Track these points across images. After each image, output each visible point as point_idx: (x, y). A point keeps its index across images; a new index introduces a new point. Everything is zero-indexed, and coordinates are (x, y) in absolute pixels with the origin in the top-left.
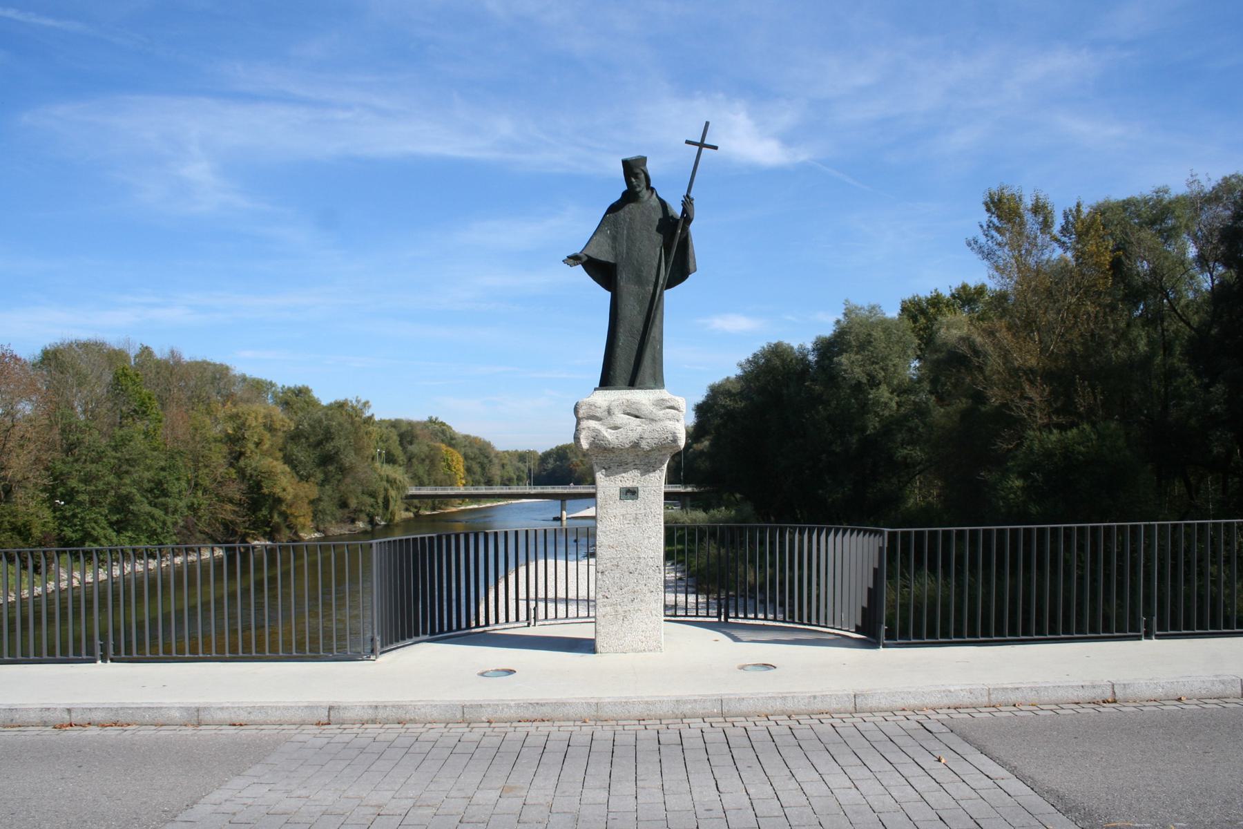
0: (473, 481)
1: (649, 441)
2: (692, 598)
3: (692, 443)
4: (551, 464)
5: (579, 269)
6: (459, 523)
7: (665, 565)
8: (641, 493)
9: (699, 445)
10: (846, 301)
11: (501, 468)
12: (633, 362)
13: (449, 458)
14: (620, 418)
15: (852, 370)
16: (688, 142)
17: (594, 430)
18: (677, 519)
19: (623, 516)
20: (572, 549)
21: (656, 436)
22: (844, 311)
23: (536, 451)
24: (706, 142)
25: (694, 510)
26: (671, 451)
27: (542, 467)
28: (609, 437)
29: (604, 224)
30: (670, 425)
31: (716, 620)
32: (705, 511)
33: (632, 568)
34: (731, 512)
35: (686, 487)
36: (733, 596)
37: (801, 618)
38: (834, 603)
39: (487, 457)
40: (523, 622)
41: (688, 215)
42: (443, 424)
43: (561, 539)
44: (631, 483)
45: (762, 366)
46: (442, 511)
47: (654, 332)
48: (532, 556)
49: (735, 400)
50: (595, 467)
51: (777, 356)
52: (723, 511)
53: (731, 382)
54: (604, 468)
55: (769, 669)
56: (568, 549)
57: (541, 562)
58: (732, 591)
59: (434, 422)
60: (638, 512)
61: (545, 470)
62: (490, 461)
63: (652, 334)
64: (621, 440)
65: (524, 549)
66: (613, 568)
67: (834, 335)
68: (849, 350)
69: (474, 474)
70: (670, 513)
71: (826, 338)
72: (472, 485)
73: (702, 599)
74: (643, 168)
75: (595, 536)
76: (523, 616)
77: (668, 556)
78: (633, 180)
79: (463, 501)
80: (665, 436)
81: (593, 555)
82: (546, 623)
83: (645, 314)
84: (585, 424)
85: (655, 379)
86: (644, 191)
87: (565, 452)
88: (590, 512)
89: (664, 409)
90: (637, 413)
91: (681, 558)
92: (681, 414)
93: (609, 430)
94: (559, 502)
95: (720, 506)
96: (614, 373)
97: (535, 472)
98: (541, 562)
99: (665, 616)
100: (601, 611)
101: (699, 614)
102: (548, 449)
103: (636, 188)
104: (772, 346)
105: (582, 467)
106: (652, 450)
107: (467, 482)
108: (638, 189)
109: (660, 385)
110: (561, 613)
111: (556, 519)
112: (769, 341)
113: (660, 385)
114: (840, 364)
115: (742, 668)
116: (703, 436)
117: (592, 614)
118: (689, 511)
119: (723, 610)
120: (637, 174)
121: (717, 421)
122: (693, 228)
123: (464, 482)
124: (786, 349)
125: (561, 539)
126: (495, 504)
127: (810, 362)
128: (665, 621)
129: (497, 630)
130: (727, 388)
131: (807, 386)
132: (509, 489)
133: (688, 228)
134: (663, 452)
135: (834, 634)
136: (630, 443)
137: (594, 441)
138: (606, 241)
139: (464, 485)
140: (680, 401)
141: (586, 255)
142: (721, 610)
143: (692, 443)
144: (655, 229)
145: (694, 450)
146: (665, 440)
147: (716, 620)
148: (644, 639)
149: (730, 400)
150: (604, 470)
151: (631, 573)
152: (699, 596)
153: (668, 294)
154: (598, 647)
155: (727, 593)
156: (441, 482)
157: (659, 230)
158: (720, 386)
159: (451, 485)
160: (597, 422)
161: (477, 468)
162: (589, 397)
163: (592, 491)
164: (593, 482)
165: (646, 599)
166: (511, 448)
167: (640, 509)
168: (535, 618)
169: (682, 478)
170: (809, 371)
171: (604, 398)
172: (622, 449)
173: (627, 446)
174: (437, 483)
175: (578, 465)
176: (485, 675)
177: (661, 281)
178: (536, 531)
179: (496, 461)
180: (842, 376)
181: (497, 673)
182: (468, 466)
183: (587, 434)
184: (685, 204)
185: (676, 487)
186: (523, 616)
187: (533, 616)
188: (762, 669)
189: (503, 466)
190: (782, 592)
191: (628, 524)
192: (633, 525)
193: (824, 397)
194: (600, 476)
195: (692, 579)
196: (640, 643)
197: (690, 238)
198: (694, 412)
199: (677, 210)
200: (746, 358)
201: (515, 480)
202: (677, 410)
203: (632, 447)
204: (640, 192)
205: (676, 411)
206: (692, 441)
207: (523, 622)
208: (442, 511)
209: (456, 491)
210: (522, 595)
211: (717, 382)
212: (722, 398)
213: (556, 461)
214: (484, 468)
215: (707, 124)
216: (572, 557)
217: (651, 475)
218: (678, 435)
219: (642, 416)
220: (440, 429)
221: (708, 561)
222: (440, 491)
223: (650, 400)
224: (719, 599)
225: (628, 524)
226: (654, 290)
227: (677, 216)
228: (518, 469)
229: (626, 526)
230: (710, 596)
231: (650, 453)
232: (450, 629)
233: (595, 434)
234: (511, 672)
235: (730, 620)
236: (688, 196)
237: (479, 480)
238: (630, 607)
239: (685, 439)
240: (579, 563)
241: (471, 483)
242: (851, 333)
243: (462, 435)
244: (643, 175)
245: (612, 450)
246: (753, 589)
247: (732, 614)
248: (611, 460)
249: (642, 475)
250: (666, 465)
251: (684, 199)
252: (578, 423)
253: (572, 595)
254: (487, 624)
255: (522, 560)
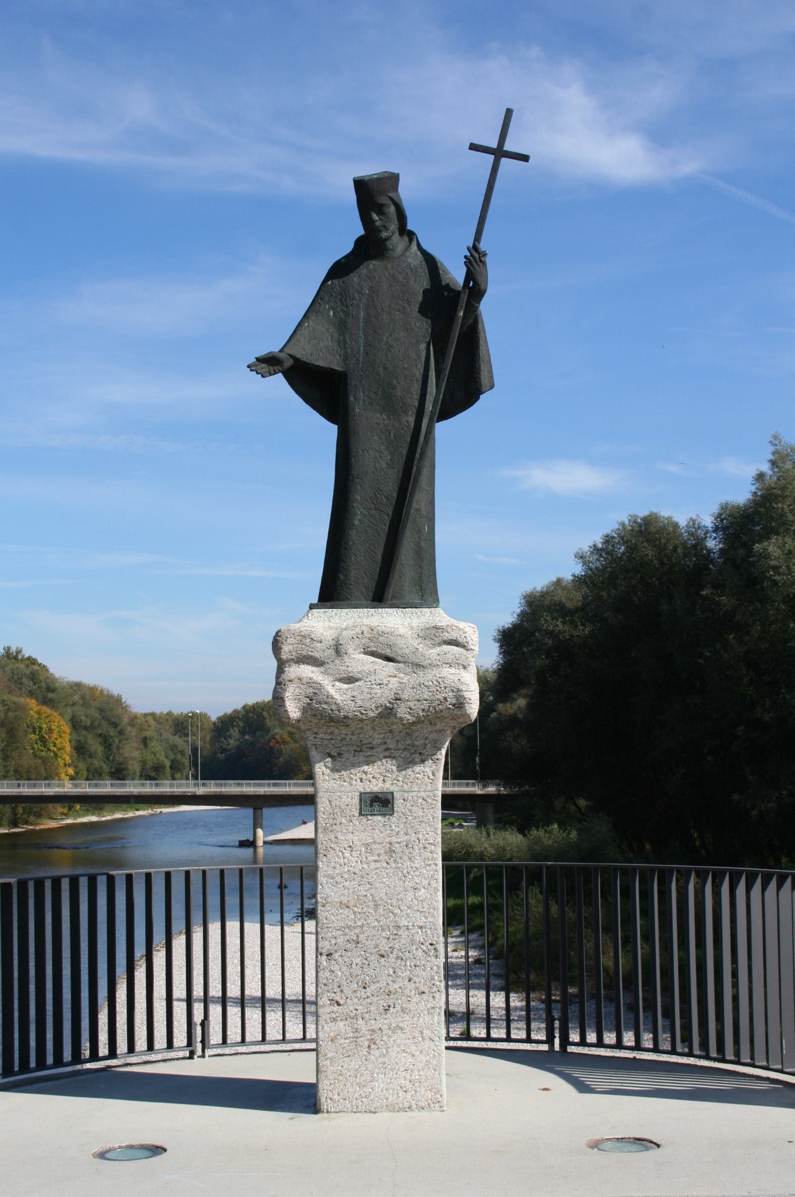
0: (88, 770)
1: (411, 704)
2: (498, 1000)
3: (495, 702)
4: (234, 740)
5: (279, 382)
6: (63, 851)
7: (446, 934)
8: (398, 803)
9: (508, 705)
10: (775, 437)
11: (142, 746)
12: (380, 556)
13: (44, 726)
14: (359, 662)
15: (788, 567)
16: (474, 147)
17: (311, 683)
18: (470, 846)
19: (367, 845)
20: (271, 902)
21: (425, 696)
22: (771, 457)
23: (206, 714)
24: (508, 147)
25: (500, 829)
26: (453, 723)
27: (217, 746)
28: (337, 697)
29: (322, 299)
30: (450, 674)
31: (545, 1047)
32: (522, 831)
33: (384, 947)
34: (569, 833)
35: (485, 786)
36: (576, 996)
37: (704, 1045)
38: (766, 1002)
39: (115, 725)
40: (180, 1049)
41: (476, 283)
42: (32, 661)
43: (251, 882)
44: (380, 784)
45: (621, 559)
46: (31, 827)
47: (418, 501)
48: (197, 917)
49: (572, 622)
50: (314, 754)
51: (648, 540)
52: (555, 832)
53: (564, 589)
54: (330, 755)
55: (647, 1149)
56: (266, 901)
57: (214, 928)
58: (573, 986)
59: (16, 658)
60: (394, 839)
61: (223, 750)
62: (121, 733)
63: (415, 505)
64: (360, 703)
65: (183, 914)
66: (349, 946)
67: (754, 501)
68: (782, 530)
69: (91, 756)
70: (457, 833)
71: (738, 507)
72: (87, 779)
73: (517, 1001)
74: (391, 195)
75: (314, 876)
76: (180, 1038)
77: (452, 918)
78: (375, 217)
79: (70, 809)
80: (441, 696)
81: (312, 914)
82: (227, 1051)
83: (401, 466)
84: (294, 671)
85: (421, 589)
86: (396, 237)
87: (260, 715)
88: (305, 832)
89: (439, 644)
90: (388, 652)
91: (477, 921)
92: (469, 654)
93: (337, 683)
94: (250, 811)
95: (547, 822)
96: (346, 576)
97: (206, 753)
98: (214, 928)
99: (448, 1038)
100: (328, 1030)
101: (513, 1036)
102: (229, 711)
103: (380, 231)
104: (639, 520)
105: (293, 745)
106: (419, 721)
107: (77, 773)
108: (384, 234)
109: (430, 599)
110: (253, 1033)
111: (243, 844)
112: (632, 513)
113: (430, 599)
114: (766, 556)
115: (596, 1145)
116: (514, 689)
117: (311, 1034)
118: (492, 831)
119: (557, 1024)
120: (382, 205)
121: (541, 662)
122: (486, 308)
123: (71, 771)
124: (664, 528)
125: (251, 882)
126: (130, 814)
127: (709, 551)
128: (447, 1048)
129: (131, 1064)
130: (557, 599)
131: (706, 598)
132: (157, 785)
133: (478, 307)
134: (438, 727)
135: (768, 1079)
136: (377, 708)
137: (309, 704)
138: (328, 330)
139: (72, 778)
140: (468, 629)
141: (290, 356)
142: (553, 1024)
143: (495, 702)
144: (417, 306)
145: (500, 714)
146: (441, 703)
147: (545, 1047)
148: (409, 1085)
149: (564, 623)
150: (329, 759)
151: (382, 956)
152: (512, 995)
153: (444, 430)
154: (323, 1100)
155: (564, 993)
156: (28, 771)
157: (424, 310)
158: (544, 595)
159: (46, 778)
160: (314, 668)
161: (96, 746)
162: (300, 621)
163: (310, 790)
164: (310, 776)
165: (412, 1006)
166: (160, 707)
167: (398, 832)
168: (203, 1042)
169: (477, 768)
170: (710, 569)
171: (327, 624)
172: (362, 720)
173: (372, 714)
174: (19, 775)
175: (284, 742)
176: (107, 1155)
177: (429, 406)
178: (204, 872)
179: (131, 732)
180: (769, 579)
181: (130, 1151)
182: (78, 741)
183: (297, 690)
184: (470, 262)
185: (467, 785)
186: (180, 1038)
187: (199, 1039)
188: (635, 1147)
189: (145, 741)
190: (667, 989)
191: (375, 861)
192: (385, 865)
193: (738, 618)
194: (321, 769)
195: (499, 962)
196: (401, 1093)
197: (480, 326)
198: (498, 645)
199: (456, 274)
200: (591, 544)
201: (168, 769)
202: (464, 647)
203: (381, 715)
204: (388, 238)
205: (461, 650)
206: (495, 699)
207: (180, 1049)
208: (31, 827)
209: (57, 790)
210: (179, 991)
211: (539, 588)
212: (548, 618)
213: (243, 733)
214: (110, 745)
215: (509, 113)
216: (272, 917)
217: (418, 768)
218: (465, 694)
219: (400, 659)
220: (28, 672)
221: (527, 927)
222: (26, 790)
223: (412, 628)
224: (548, 1002)
225: (375, 861)
226: (415, 422)
227: (456, 283)
228: (173, 747)
229: (373, 865)
230: (531, 995)
231: (414, 728)
232: (41, 1064)
233: (311, 690)
234: (157, 1150)
235: (571, 1049)
236: (475, 248)
237: (101, 768)
238: (382, 1022)
239: (478, 703)
240: (286, 928)
241: (85, 773)
242: (784, 497)
243: (68, 683)
244: (392, 209)
245: (345, 721)
246: (612, 984)
247: (575, 1037)
248: (343, 739)
249: (400, 768)
250: (444, 751)
251: (468, 254)
252: (280, 671)
253: (273, 991)
254: (113, 1054)
255: (178, 924)
